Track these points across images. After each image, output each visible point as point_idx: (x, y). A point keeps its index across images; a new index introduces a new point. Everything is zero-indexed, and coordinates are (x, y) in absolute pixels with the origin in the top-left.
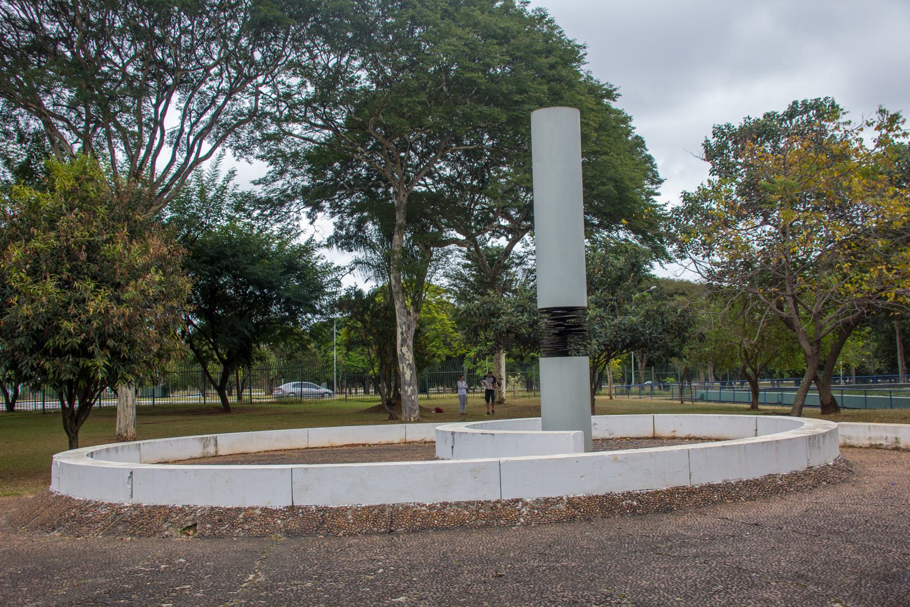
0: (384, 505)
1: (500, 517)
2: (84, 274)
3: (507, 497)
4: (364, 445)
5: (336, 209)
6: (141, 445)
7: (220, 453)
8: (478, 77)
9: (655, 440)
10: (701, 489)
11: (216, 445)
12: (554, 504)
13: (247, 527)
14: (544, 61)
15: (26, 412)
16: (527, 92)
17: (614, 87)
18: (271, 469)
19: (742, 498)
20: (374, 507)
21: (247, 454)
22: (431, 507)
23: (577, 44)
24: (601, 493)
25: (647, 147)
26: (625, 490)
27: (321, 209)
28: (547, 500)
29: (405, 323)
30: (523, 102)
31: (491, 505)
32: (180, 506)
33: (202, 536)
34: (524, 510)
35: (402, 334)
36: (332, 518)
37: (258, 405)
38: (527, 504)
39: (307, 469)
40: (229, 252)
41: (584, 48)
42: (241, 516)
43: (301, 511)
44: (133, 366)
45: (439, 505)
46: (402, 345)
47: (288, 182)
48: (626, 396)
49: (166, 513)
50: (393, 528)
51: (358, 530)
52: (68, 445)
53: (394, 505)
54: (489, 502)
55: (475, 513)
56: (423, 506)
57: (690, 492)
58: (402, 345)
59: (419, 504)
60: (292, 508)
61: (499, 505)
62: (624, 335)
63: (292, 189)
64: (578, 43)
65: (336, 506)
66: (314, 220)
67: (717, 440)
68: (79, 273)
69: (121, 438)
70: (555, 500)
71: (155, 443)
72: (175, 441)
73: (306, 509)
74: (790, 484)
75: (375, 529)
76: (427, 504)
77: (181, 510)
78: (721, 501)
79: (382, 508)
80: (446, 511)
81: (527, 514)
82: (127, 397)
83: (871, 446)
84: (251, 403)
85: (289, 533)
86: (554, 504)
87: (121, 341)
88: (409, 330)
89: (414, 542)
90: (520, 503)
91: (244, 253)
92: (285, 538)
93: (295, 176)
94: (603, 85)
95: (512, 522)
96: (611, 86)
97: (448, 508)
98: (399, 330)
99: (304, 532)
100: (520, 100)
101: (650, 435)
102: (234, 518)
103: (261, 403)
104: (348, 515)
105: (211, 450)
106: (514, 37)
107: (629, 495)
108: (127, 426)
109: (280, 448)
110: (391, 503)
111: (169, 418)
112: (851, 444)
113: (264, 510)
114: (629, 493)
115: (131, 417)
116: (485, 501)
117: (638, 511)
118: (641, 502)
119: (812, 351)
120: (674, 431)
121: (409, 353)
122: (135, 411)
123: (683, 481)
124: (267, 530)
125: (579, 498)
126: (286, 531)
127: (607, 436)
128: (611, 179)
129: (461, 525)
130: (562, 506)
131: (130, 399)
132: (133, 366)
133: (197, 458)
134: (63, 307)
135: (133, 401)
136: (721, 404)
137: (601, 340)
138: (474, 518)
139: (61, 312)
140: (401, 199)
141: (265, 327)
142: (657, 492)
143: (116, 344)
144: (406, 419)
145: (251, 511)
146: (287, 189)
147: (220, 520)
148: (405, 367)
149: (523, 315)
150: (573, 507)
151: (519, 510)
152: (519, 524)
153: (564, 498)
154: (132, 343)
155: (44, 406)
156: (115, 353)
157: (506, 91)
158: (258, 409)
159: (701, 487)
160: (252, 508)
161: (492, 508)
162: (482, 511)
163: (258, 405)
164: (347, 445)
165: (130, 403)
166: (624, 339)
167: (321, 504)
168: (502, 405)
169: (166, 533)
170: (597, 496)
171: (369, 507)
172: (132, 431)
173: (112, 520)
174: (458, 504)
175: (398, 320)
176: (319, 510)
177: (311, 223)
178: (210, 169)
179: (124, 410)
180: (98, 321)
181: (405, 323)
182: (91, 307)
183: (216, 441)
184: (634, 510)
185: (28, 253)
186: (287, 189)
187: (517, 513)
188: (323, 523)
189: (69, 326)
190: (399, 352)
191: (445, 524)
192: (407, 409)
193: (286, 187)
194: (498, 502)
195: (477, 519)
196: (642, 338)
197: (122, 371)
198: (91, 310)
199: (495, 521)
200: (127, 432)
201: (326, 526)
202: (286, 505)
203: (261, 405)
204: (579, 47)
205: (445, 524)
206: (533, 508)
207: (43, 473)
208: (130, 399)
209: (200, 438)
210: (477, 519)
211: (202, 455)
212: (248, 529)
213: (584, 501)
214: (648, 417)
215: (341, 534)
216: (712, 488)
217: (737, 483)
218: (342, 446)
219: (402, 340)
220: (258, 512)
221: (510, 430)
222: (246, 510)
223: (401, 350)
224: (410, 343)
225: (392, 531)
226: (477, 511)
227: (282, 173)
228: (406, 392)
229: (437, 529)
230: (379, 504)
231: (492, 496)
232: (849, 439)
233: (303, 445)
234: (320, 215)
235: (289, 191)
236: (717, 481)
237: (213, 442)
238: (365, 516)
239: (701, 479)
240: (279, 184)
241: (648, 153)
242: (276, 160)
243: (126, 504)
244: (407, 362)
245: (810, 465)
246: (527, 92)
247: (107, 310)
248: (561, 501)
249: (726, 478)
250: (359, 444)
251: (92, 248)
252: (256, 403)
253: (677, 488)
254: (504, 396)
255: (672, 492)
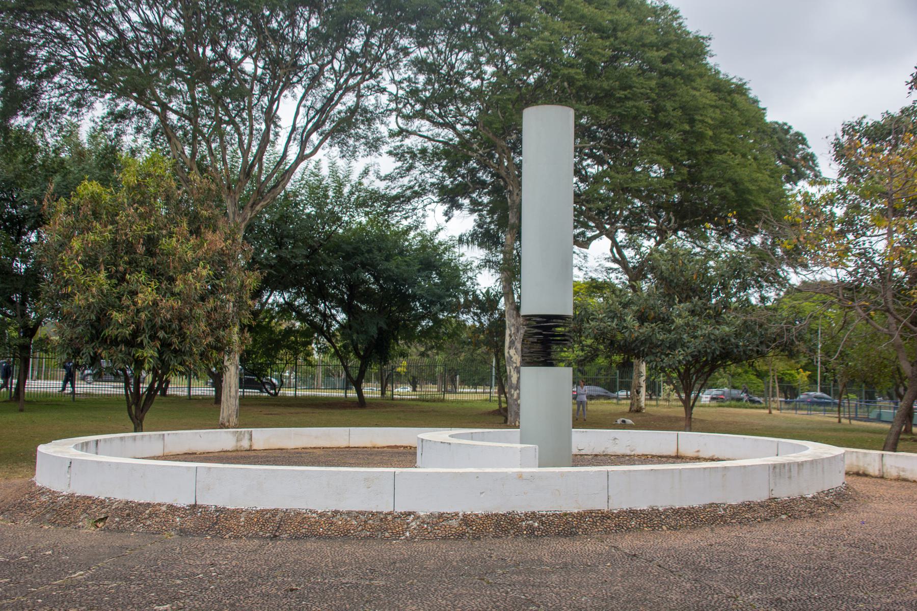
0: (278, 509)
1: (386, 530)
2: (141, 267)
3: (400, 509)
4: (405, 447)
5: (475, 207)
6: (166, 436)
7: (254, 448)
8: (577, 73)
9: (678, 458)
10: (618, 515)
11: (251, 439)
12: (447, 519)
13: (148, 523)
14: (654, 54)
15: (177, 397)
16: (630, 87)
17: (744, 81)
18: (179, 467)
19: (664, 527)
20: (268, 511)
21: (282, 449)
22: (321, 515)
23: (701, 35)
24: (502, 511)
25: (809, 143)
26: (529, 510)
27: (460, 207)
28: (441, 515)
29: (514, 325)
30: (627, 98)
31: (382, 516)
32: (103, 498)
33: (108, 529)
34: (414, 523)
35: (510, 336)
36: (225, 519)
37: (399, 402)
38: (419, 517)
39: (210, 468)
40: (364, 248)
41: (710, 39)
42: (147, 512)
43: (200, 510)
44: (185, 358)
45: (329, 513)
46: (510, 348)
47: (416, 179)
48: (794, 412)
49: (84, 504)
50: (277, 534)
51: (245, 533)
52: (133, 429)
53: (287, 510)
54: (381, 513)
55: (363, 523)
56: (315, 513)
57: (604, 516)
58: (510, 348)
59: (311, 511)
60: (194, 507)
61: (390, 517)
62: (715, 345)
63: (420, 186)
64: (702, 34)
65: (233, 508)
66: (449, 218)
67: (712, 460)
68: (137, 266)
69: (223, 426)
70: (450, 516)
71: (182, 434)
72: (205, 433)
73: (205, 508)
74: (733, 516)
75: (261, 533)
76: (319, 512)
77: (102, 502)
78: (639, 528)
79: (275, 512)
80: (335, 520)
81: (414, 529)
82: (230, 387)
83: (898, 479)
84: (393, 399)
85: (183, 532)
86: (447, 519)
87: (173, 332)
88: (518, 332)
89: (294, 546)
90: (412, 516)
91: (380, 250)
92: (177, 536)
93: (422, 173)
94: (731, 79)
95: (396, 536)
96: (741, 80)
97: (338, 517)
98: (508, 332)
99: (198, 532)
100: (623, 96)
101: (673, 453)
102: (141, 514)
103: (403, 399)
104: (241, 517)
105: (245, 444)
106: (623, 31)
107: (533, 516)
108: (230, 415)
109: (319, 446)
110: (284, 508)
111: (292, 410)
112: (905, 477)
113: (170, 507)
114: (533, 513)
115: (233, 408)
116: (377, 512)
117: (536, 533)
118: (543, 523)
119: (912, 372)
120: (698, 451)
121: (517, 356)
122: (237, 401)
123: (600, 505)
124: (164, 527)
125: (476, 515)
126: (180, 530)
127: (628, 452)
128: (729, 180)
129: (346, 535)
130: (454, 523)
131: (233, 390)
132: (185, 358)
133: (229, 451)
134: (118, 297)
135: (237, 392)
136: (868, 424)
137: (689, 351)
138: (360, 528)
139: (116, 302)
140: (515, 198)
141: (405, 323)
142: (565, 514)
143: (166, 336)
144: (511, 423)
145: (158, 507)
146: (414, 186)
147: (128, 515)
148: (512, 370)
149: (613, 322)
150: (466, 524)
151: (408, 524)
152: (403, 538)
153: (460, 514)
154: (183, 337)
155: (346, 393)
156: (166, 345)
157: (606, 87)
158: (396, 405)
159: (620, 511)
160: (159, 504)
161: (381, 520)
162: (370, 522)
163: (399, 402)
164: (388, 447)
165: (233, 393)
166: (714, 349)
167: (220, 505)
168: (639, 414)
169: (80, 524)
170: (496, 515)
171: (263, 511)
172: (234, 420)
173: (45, 508)
174: (349, 513)
175: (507, 322)
176: (218, 510)
177: (447, 221)
178: (344, 165)
179: (227, 400)
180: (147, 313)
181: (514, 325)
182: (140, 299)
183: (251, 435)
184: (531, 530)
185: (90, 245)
186: (414, 186)
187: (406, 526)
188: (216, 523)
189: (118, 317)
190: (506, 354)
191: (330, 533)
192: (513, 413)
193: (412, 183)
194: (390, 513)
195: (363, 530)
196: (735, 350)
197: (174, 363)
198: (139, 301)
199: (380, 533)
200: (229, 421)
201: (217, 527)
202: (189, 504)
203: (401, 402)
204: (703, 38)
205: (330, 533)
206: (423, 522)
207: (29, 459)
208: (233, 390)
209: (233, 432)
210: (363, 530)
211: (235, 449)
212: (149, 525)
213: (480, 519)
214: (671, 435)
215: (227, 536)
216: (633, 513)
217: (665, 510)
218: (384, 447)
219: (510, 342)
220: (164, 508)
221: (499, 442)
222: (154, 506)
223: (509, 352)
224: (519, 346)
225: (275, 536)
226: (365, 522)
227: (411, 168)
228: (512, 395)
229: (320, 537)
230: (273, 508)
231: (385, 507)
232: (903, 471)
233: (344, 444)
234: (456, 212)
235: (416, 188)
236: (642, 505)
237: (247, 436)
238: (256, 520)
239: (619, 503)
240: (405, 181)
241: (810, 151)
242: (404, 156)
243: (65, 493)
244: (515, 365)
245: (773, 496)
246: (630, 87)
247: (155, 303)
248: (456, 517)
249: (652, 504)
250: (401, 447)
251: (151, 242)
252: (397, 399)
253: (591, 512)
254: (643, 404)
255: (581, 516)
